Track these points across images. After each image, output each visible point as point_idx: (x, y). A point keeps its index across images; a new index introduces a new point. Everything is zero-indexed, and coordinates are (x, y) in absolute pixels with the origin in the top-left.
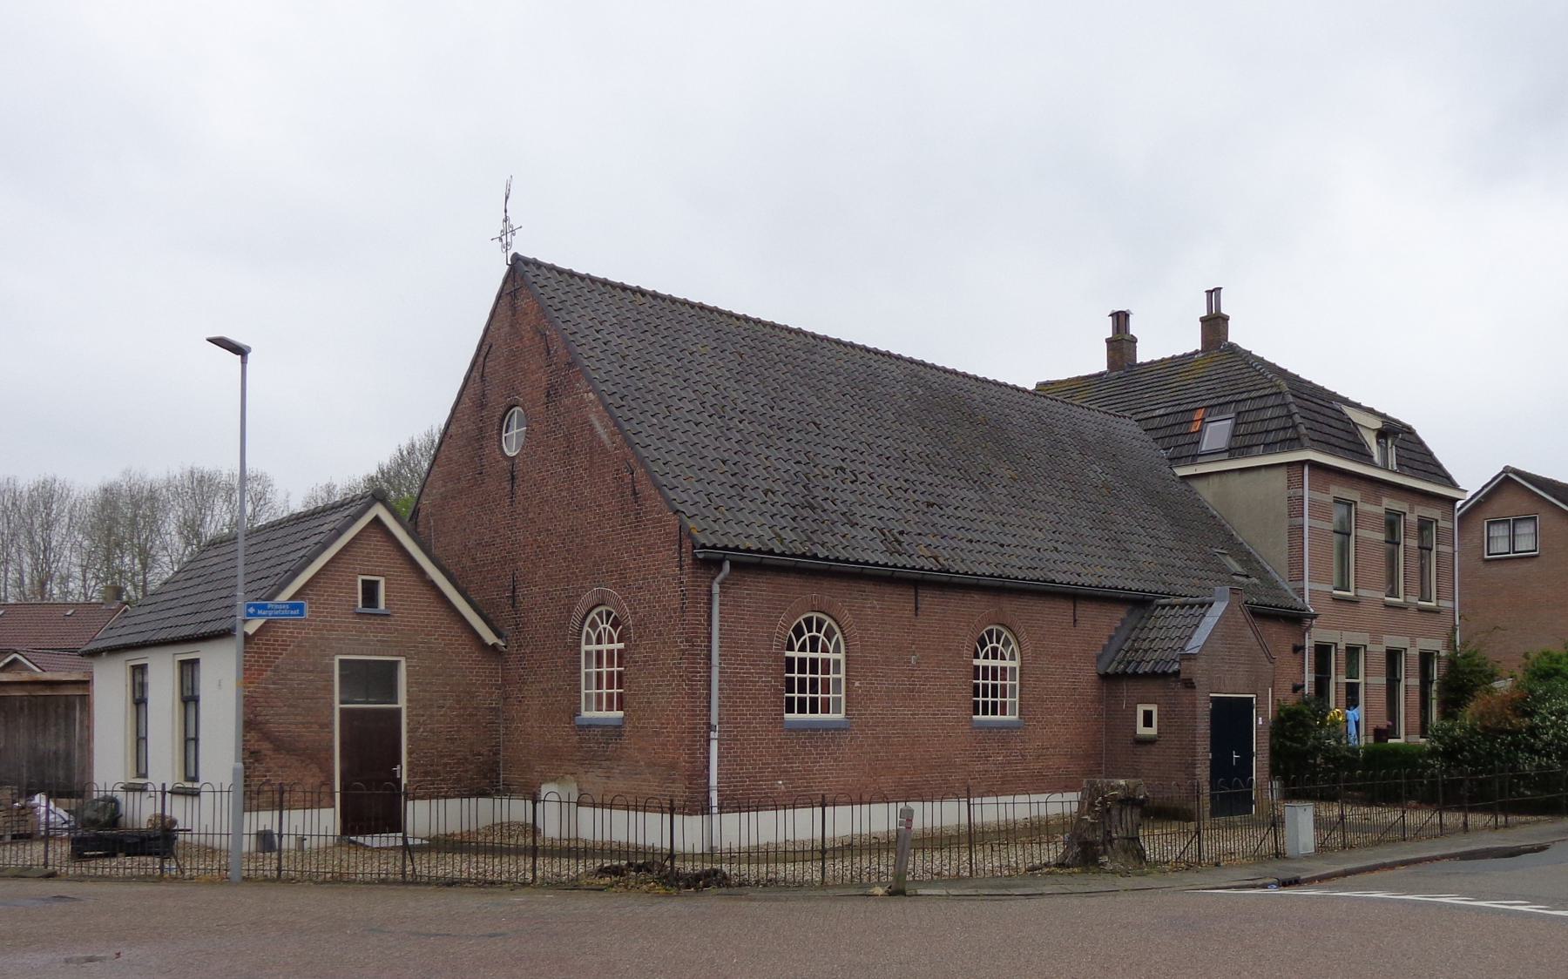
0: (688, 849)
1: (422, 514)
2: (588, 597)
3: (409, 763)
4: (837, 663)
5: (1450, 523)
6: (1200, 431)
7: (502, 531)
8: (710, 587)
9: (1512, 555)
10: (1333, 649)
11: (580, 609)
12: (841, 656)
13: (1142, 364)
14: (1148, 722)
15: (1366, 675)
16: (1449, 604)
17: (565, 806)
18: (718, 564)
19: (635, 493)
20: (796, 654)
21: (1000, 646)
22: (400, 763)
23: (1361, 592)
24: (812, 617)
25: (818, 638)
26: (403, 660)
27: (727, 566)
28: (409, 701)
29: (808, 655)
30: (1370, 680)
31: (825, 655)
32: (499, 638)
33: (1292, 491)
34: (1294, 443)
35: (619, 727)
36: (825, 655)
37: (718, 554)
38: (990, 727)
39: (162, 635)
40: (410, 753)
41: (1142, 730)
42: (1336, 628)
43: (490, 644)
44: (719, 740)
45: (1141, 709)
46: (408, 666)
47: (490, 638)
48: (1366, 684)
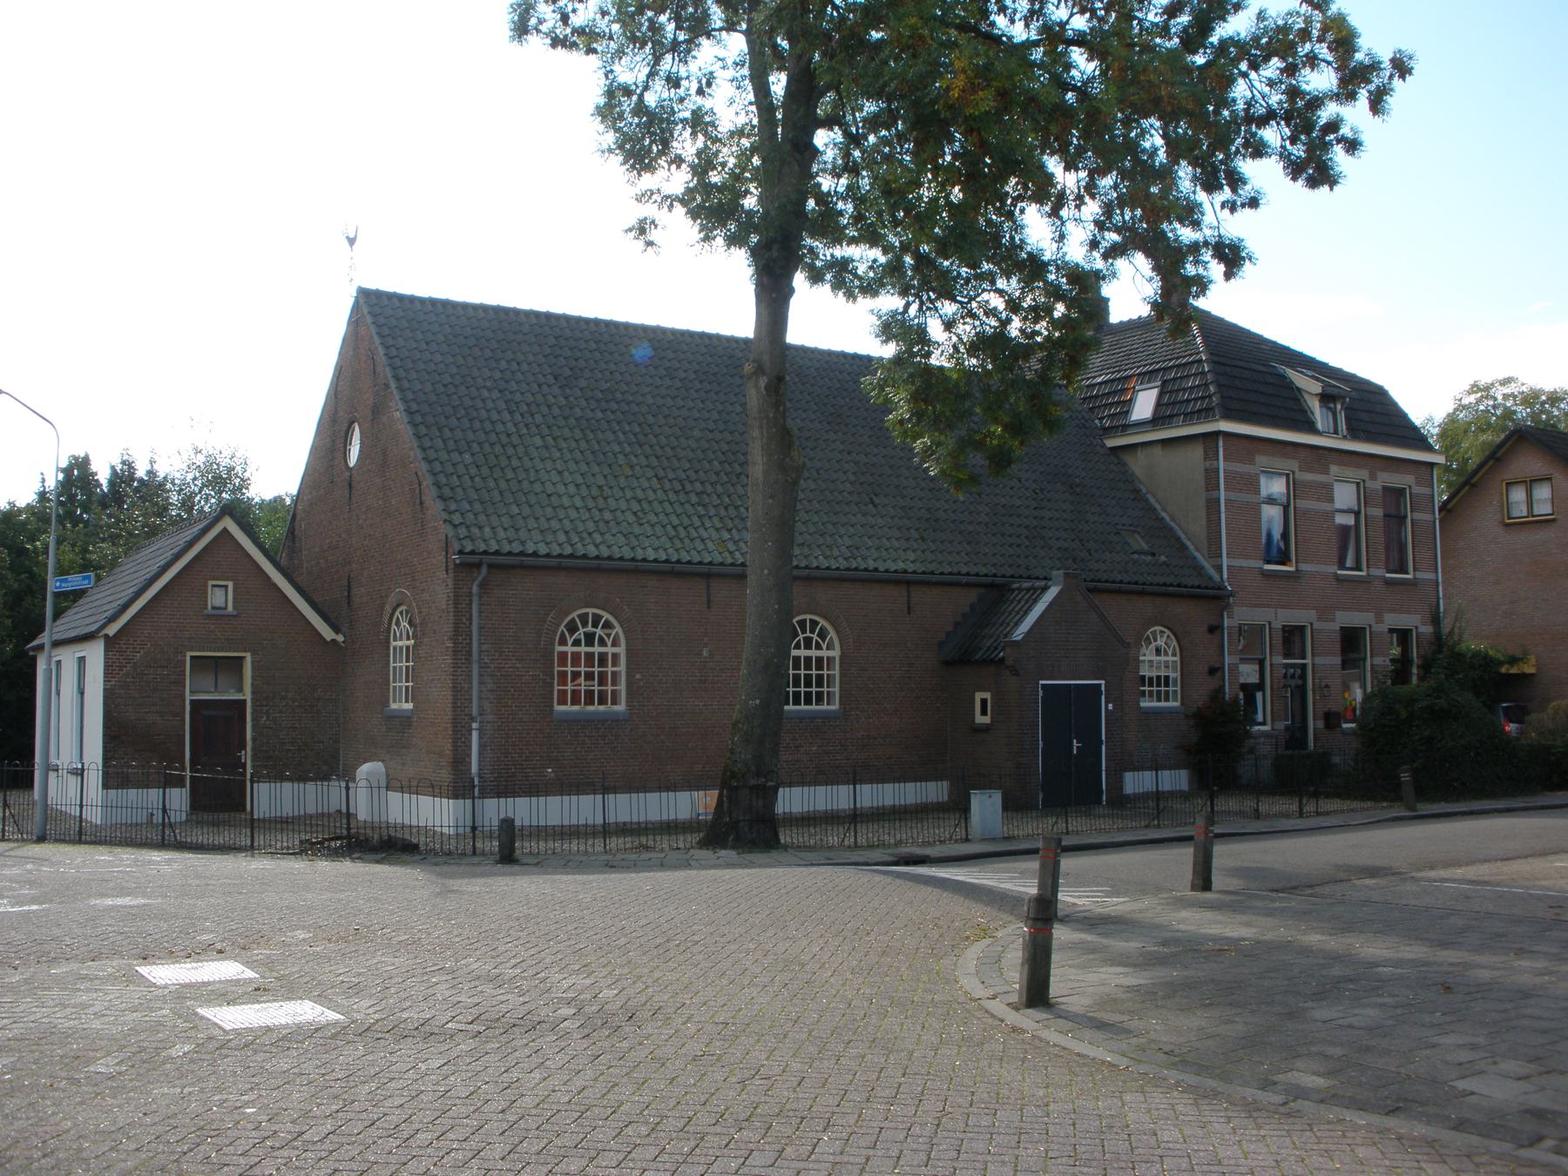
0: (261, 816)
1: (298, 518)
2: (393, 599)
3: (253, 749)
4: (615, 656)
5: (1428, 489)
6: (1131, 400)
7: (343, 535)
8: (471, 588)
9: (1531, 519)
10: (1368, 630)
11: (388, 609)
12: (621, 650)
13: (1112, 325)
14: (984, 712)
15: (1313, 655)
16: (1430, 576)
17: (375, 791)
18: (478, 566)
19: (421, 503)
20: (569, 649)
21: (815, 637)
22: (245, 749)
23: (1303, 567)
24: (573, 619)
25: (594, 634)
26: (794, 621)
27: (484, 570)
28: (253, 693)
29: (583, 649)
30: (1318, 660)
31: (603, 649)
32: (337, 633)
33: (1208, 463)
34: (1206, 413)
35: (408, 717)
36: (603, 649)
37: (474, 559)
38: (813, 717)
39: (73, 634)
40: (254, 739)
41: (980, 719)
42: (1269, 606)
43: (328, 640)
44: (480, 730)
45: (979, 696)
46: (253, 662)
47: (327, 633)
48: (1313, 665)
